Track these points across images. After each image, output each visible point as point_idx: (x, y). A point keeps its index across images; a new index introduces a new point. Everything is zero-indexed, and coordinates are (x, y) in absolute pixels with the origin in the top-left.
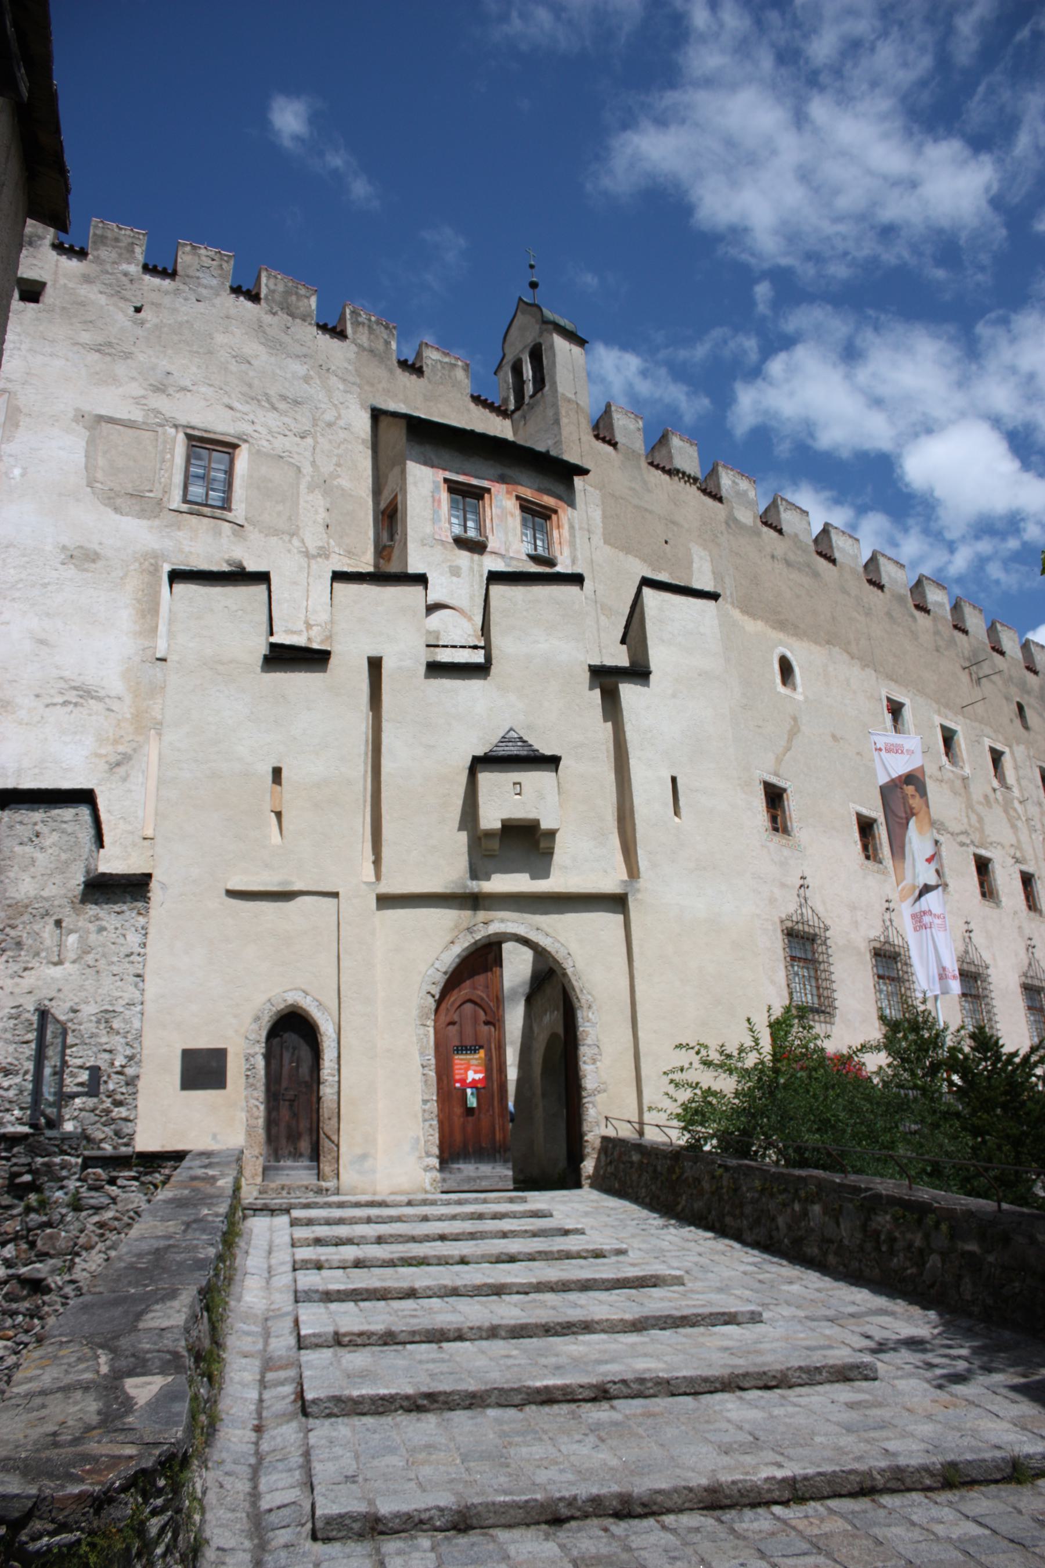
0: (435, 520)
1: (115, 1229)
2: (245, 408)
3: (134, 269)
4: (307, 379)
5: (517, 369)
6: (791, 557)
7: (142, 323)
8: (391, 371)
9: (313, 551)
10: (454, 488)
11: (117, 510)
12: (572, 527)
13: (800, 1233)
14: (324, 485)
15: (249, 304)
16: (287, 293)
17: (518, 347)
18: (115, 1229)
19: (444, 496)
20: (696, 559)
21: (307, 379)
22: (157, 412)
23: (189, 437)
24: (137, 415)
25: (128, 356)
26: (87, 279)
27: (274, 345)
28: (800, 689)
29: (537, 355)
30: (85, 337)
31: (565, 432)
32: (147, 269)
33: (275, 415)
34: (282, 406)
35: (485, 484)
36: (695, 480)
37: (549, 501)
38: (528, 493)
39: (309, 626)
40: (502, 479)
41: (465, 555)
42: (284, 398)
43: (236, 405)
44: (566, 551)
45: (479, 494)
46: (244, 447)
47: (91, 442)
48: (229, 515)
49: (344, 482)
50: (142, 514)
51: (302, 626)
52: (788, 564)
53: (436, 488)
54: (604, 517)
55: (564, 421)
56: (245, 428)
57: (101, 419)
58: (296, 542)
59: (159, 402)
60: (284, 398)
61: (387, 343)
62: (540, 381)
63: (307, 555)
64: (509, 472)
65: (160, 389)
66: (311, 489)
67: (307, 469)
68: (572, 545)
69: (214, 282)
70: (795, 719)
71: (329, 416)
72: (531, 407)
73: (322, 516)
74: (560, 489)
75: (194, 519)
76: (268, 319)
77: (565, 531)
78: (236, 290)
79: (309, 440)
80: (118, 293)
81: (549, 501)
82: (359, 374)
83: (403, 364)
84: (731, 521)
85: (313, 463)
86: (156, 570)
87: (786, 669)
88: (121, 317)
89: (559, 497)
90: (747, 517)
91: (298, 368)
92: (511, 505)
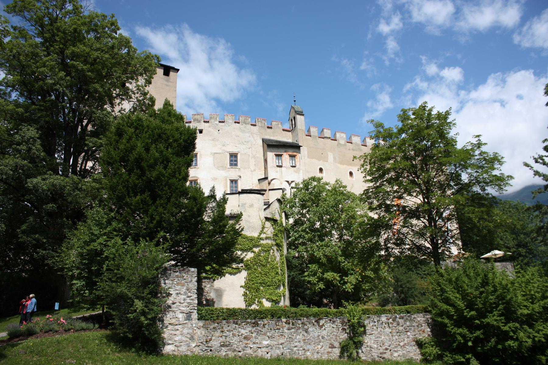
0: (273, 163)
1: (59, 324)
2: (239, 146)
3: (217, 122)
4: (249, 137)
5: (292, 120)
6: (354, 148)
7: (220, 133)
8: (266, 130)
9: (253, 170)
10: (276, 155)
11: (219, 170)
12: (300, 158)
13: (143, 295)
14: (254, 157)
15: (238, 124)
16: (245, 120)
17: (292, 117)
18: (59, 324)
19: (275, 157)
20: (329, 155)
21: (249, 137)
22: (224, 150)
23: (230, 154)
24: (221, 151)
25: (218, 140)
26: (210, 127)
27: (243, 131)
28: (354, 178)
29: (294, 118)
30: (211, 138)
31: (299, 136)
32: (219, 122)
33: (244, 146)
34: (245, 143)
35: (282, 153)
36: (330, 138)
37: (295, 154)
38: (290, 153)
39: (253, 184)
40: (285, 152)
41: (279, 168)
42: (245, 142)
43: (237, 146)
44: (298, 163)
45: (281, 155)
46: (239, 154)
47: (214, 158)
48: (237, 167)
49: (257, 155)
50: (223, 170)
51: (251, 185)
52: (353, 150)
53: (273, 156)
54: (308, 152)
55: (299, 134)
56: (239, 150)
57: (215, 153)
58: (250, 169)
59: (224, 148)
60: (245, 142)
61: (265, 124)
62: (295, 127)
63: (252, 171)
64: (286, 150)
65: (224, 145)
66: (252, 158)
67: (251, 155)
68: (300, 161)
69: (231, 121)
70: (353, 184)
71: (254, 143)
72: (294, 130)
73: (254, 163)
74: (297, 150)
75: (232, 169)
76: (242, 126)
77: (298, 159)
78: (235, 122)
79: (251, 149)
80: (215, 128)
81: (295, 154)
82: (259, 132)
83: (268, 127)
84: (339, 144)
85: (252, 153)
86: (226, 179)
87: (351, 174)
88: (216, 132)
89: (297, 152)
90: (342, 142)
91: (248, 135)
92: (288, 157)
